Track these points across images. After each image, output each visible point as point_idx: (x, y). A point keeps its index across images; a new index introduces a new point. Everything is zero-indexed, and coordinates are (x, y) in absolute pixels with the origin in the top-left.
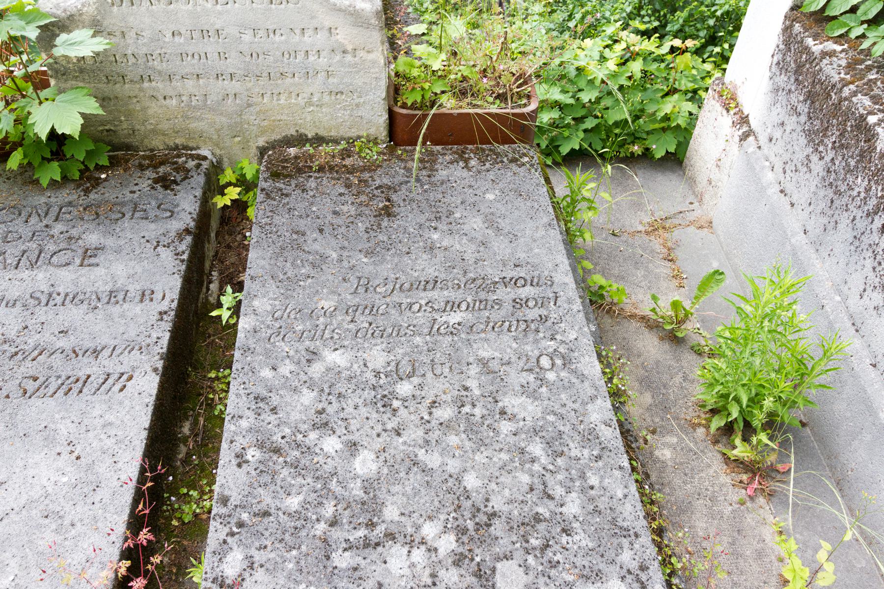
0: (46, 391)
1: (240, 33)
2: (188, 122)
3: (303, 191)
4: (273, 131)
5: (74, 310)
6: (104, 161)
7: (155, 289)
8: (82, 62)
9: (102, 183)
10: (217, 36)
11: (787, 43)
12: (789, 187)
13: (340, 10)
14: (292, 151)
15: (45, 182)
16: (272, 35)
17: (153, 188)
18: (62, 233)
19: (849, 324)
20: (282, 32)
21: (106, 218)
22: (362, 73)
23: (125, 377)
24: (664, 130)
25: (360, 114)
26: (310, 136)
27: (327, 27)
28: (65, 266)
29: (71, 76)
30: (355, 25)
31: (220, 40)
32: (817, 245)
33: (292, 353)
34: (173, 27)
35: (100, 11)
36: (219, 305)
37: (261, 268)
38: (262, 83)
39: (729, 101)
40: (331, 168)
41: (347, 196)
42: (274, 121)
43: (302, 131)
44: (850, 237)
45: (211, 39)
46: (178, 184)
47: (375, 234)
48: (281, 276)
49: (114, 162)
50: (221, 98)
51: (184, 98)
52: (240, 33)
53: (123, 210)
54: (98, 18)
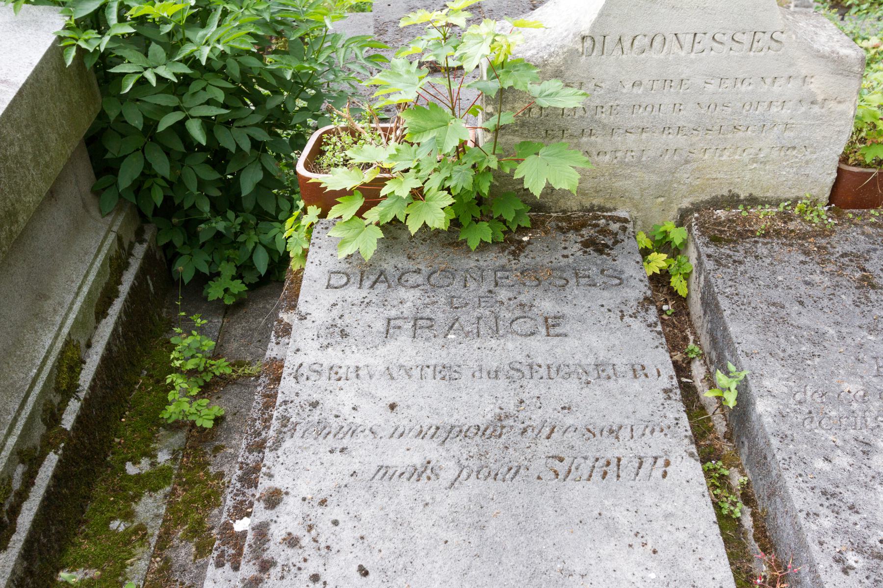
0: (579, 473)
1: (706, 83)
2: (614, 180)
3: (756, 257)
4: (703, 190)
5: (566, 385)
6: (526, 223)
7: (645, 363)
8: (527, 116)
9: (526, 246)
10: (679, 87)
13: (823, 57)
14: (721, 214)
15: (474, 244)
16: (739, 85)
17: (585, 252)
18: (510, 299)
20: (751, 81)
21: (550, 284)
22: (824, 126)
23: (661, 462)
25: (807, 173)
26: (742, 197)
27: (803, 75)
28: (530, 335)
29: (510, 131)
30: (835, 73)
31: (681, 91)
33: (839, 442)
34: (636, 77)
35: (567, 61)
37: (752, 344)
38: (710, 137)
40: (778, 233)
41: (811, 265)
42: (708, 179)
43: (736, 191)
45: (672, 90)
46: (611, 249)
47: (868, 309)
48: (782, 355)
49: (536, 224)
50: (659, 153)
51: (619, 154)
52: (706, 83)
53: (565, 275)
54: (563, 68)
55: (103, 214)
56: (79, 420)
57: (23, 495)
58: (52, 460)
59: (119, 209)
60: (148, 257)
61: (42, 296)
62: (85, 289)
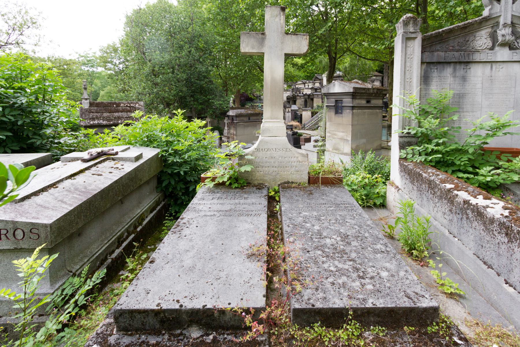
11: (401, 166)
12: (411, 197)
19: (433, 219)
24: (378, 197)
30: (302, 156)
32: (421, 206)
34: (266, 156)
36: (276, 207)
39: (393, 184)
44: (426, 199)
55: (157, 192)
56: (141, 230)
57: (125, 240)
58: (133, 236)
59: (161, 192)
60: (164, 204)
61: (140, 203)
62: (149, 205)
